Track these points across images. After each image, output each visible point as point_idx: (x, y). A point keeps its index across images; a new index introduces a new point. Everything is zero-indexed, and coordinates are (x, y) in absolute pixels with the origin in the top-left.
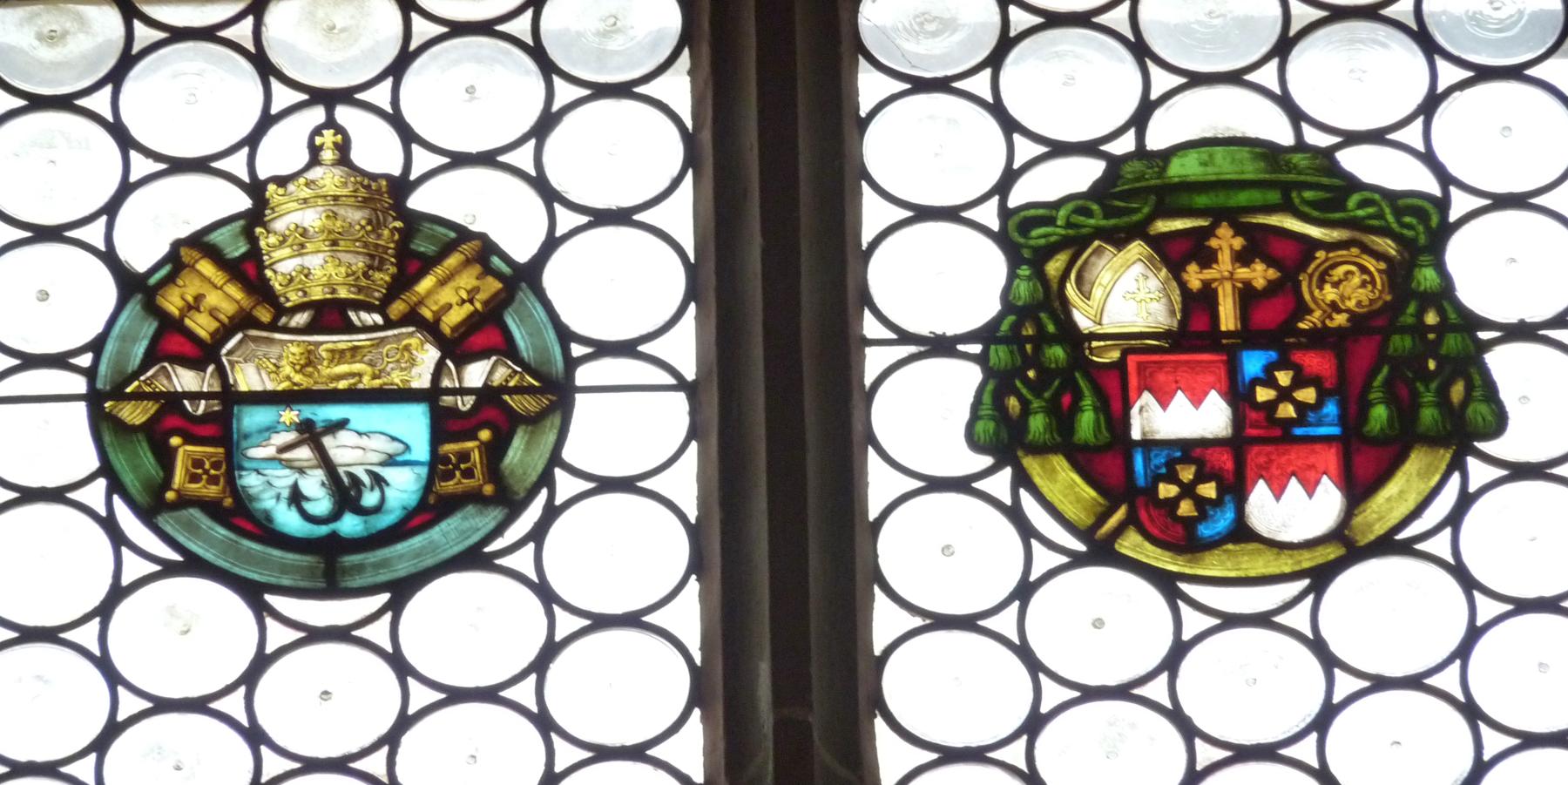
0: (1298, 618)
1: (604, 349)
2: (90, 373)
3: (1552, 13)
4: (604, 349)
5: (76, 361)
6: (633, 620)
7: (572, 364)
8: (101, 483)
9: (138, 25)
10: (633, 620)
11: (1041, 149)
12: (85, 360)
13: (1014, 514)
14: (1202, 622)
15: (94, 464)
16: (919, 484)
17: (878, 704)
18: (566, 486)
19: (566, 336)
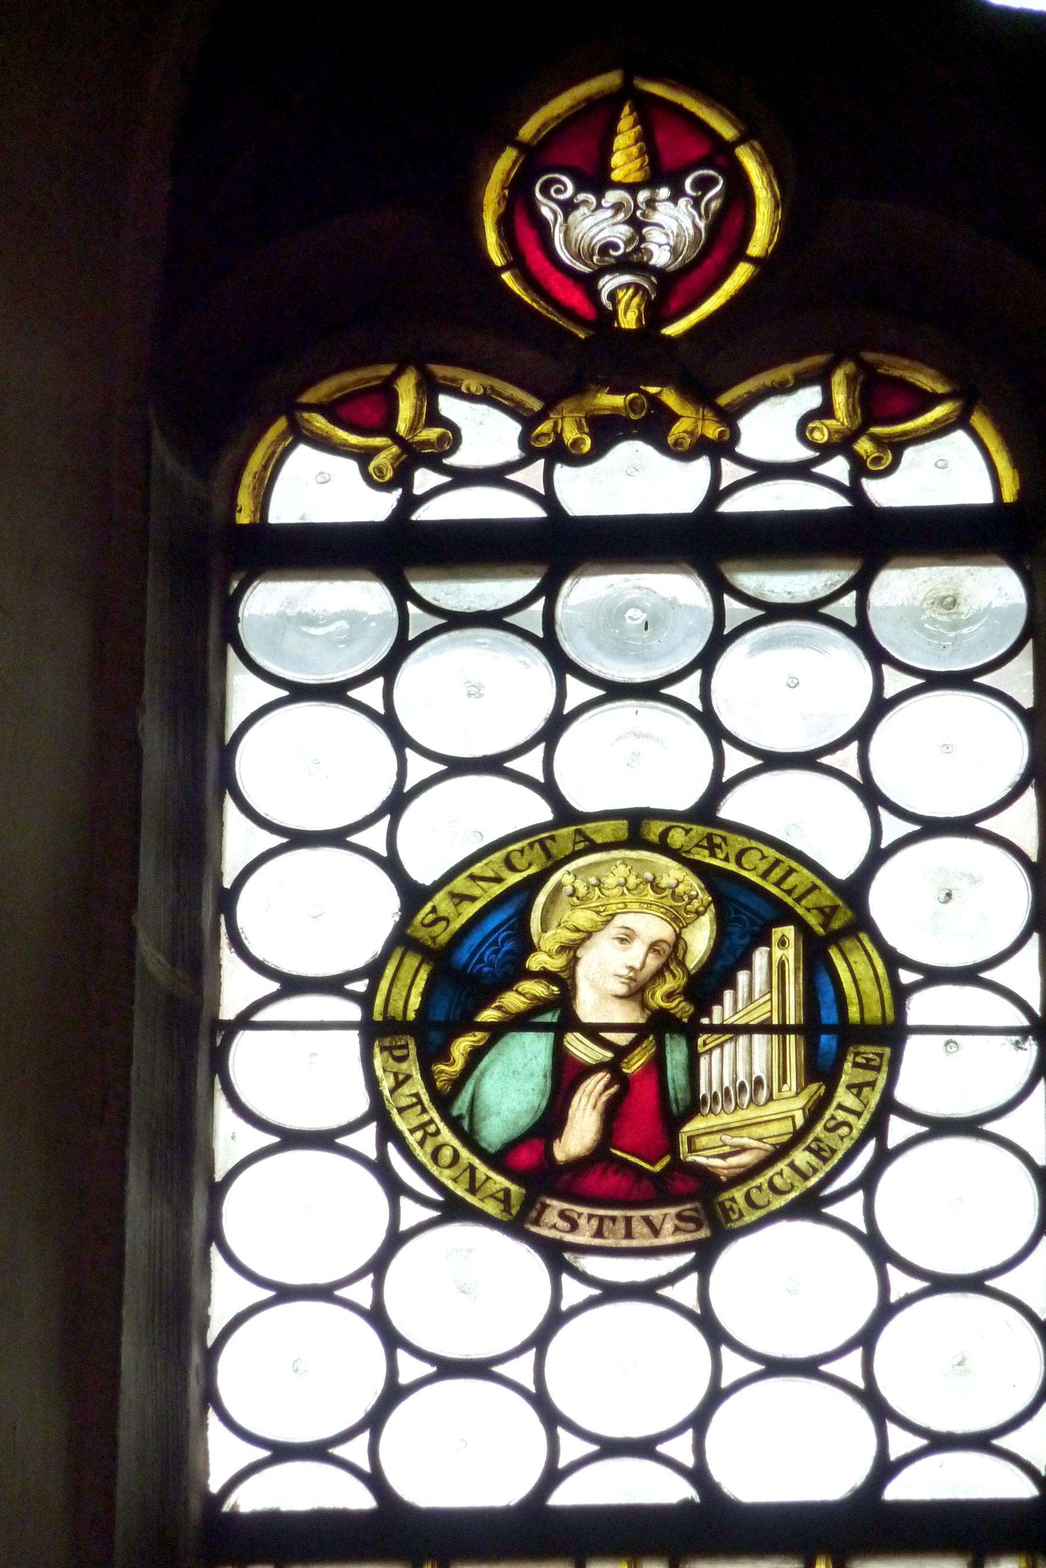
0: (685, 1292)
1: (935, 976)
2: (366, 1001)
3: (1014, 607)
4: (935, 976)
5: (351, 987)
6: (285, 1293)
7: (901, 994)
8: (372, 1129)
9: (728, 601)
10: (285, 1293)
11: (540, 749)
12: (360, 986)
13: (381, 1169)
14: (583, 1292)
15: (362, 1104)
16: (990, 1127)
17: (211, 1398)
18: (898, 1130)
19: (894, 960)
